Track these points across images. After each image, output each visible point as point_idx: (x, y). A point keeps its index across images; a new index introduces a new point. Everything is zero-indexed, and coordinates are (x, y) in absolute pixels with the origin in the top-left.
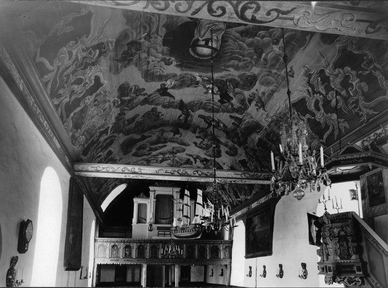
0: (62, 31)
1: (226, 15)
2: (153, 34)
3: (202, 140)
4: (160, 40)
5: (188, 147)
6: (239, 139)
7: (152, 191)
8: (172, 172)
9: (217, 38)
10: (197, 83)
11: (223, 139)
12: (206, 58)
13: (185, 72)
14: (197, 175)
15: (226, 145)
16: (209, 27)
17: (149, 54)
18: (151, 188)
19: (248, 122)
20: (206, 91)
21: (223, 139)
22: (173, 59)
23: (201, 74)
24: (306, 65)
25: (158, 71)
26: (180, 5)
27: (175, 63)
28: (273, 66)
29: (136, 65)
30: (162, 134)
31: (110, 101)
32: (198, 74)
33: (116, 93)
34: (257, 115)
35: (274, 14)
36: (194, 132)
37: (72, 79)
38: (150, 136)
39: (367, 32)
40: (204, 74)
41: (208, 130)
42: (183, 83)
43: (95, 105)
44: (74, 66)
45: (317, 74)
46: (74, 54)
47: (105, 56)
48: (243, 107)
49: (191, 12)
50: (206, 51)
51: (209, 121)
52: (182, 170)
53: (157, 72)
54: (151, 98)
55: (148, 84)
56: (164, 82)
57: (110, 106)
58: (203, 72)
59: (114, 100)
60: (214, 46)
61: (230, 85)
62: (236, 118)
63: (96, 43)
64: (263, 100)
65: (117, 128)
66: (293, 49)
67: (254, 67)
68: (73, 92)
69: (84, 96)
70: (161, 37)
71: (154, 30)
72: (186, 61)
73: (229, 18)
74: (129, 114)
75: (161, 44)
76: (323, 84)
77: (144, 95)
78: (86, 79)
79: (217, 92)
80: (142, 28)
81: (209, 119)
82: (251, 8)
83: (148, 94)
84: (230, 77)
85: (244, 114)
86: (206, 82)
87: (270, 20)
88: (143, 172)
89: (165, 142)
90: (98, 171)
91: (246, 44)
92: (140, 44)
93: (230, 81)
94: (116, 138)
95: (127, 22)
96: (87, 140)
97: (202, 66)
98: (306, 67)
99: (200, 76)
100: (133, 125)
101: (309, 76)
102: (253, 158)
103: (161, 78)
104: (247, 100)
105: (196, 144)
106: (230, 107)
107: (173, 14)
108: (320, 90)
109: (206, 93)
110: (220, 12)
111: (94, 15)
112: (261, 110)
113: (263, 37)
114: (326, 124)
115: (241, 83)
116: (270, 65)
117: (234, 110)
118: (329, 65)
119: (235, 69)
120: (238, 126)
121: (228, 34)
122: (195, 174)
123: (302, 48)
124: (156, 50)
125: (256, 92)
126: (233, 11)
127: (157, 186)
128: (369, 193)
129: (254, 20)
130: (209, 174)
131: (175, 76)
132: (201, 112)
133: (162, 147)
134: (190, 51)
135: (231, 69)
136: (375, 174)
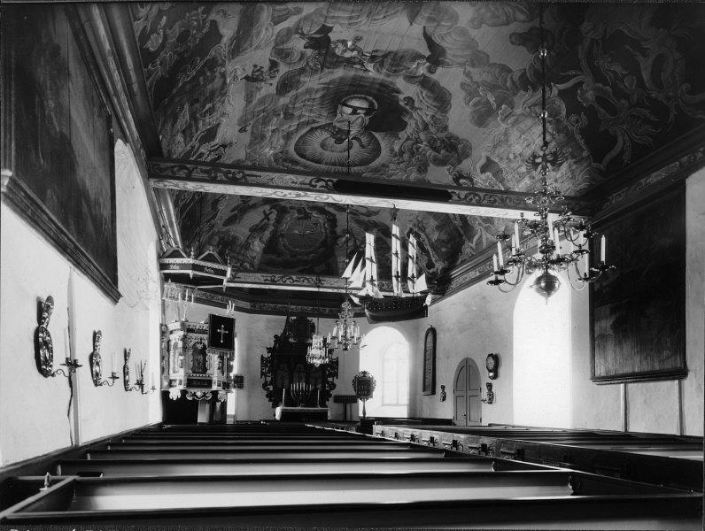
4: (409, 130)
10: (373, 58)
13: (390, 79)
17: (426, 126)
20: (359, 44)
22: (402, 103)
27: (401, 97)
40: (361, 73)
50: (356, 103)
53: (429, 97)
60: (345, 109)
85: (274, 37)
99: (366, 70)
103: (425, 83)
109: (357, 39)
124: (416, 124)
125: (271, 82)
135: (316, 87)
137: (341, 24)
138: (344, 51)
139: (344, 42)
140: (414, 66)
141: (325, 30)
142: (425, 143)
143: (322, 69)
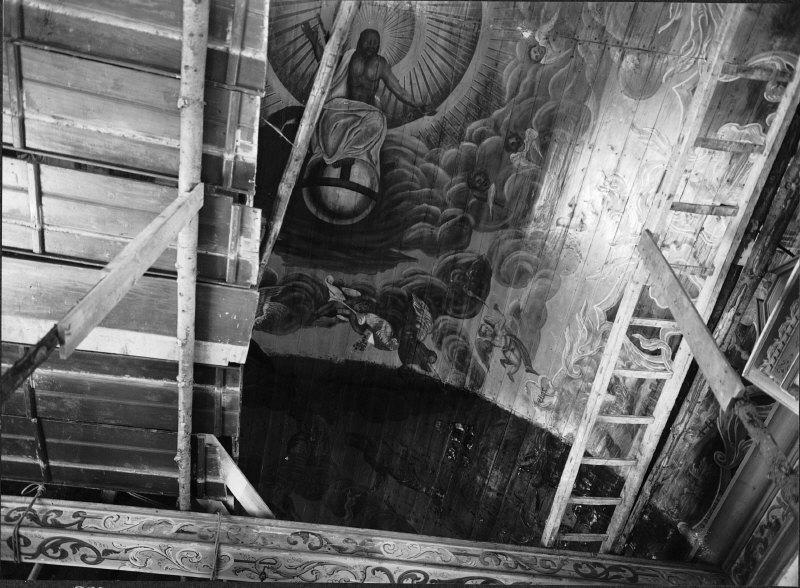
9: (370, 157)
10: (333, 310)
12: (349, 222)
13: (296, 270)
20: (359, 339)
50: (345, 198)
61: (420, 310)
67: (474, 232)
86: (357, 306)
113: (480, 137)
138: (378, 327)
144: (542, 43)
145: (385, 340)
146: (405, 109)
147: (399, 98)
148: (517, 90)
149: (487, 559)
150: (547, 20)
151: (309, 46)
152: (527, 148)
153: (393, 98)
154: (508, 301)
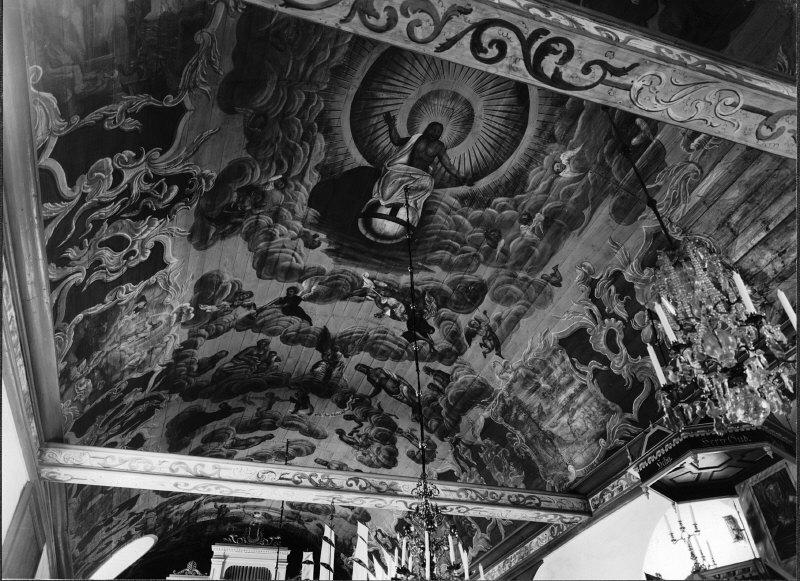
0: (115, 122)
1: (506, 62)
2: (293, 179)
3: (356, 425)
4: (303, 195)
5: (323, 442)
6: (440, 420)
7: (219, 557)
8: (296, 478)
9: (416, 204)
10: (364, 293)
11: (405, 422)
12: (389, 242)
13: (342, 267)
14: (355, 487)
15: (410, 437)
16: (402, 183)
17: (277, 217)
18: (217, 549)
19: (463, 383)
20: (379, 311)
21: (405, 422)
22: (323, 236)
23: (375, 273)
24: (585, 263)
25: (286, 259)
26: (419, 23)
27: (324, 245)
28: (519, 264)
29: (247, 239)
30: (270, 408)
31: (172, 308)
32: (367, 274)
33: (188, 293)
34: (485, 365)
35: (597, 71)
36: (341, 405)
37: (106, 233)
38: (241, 409)
39: (759, 136)
40: (379, 275)
41: (373, 400)
42: (336, 290)
43: (137, 310)
44: (118, 206)
45: (608, 278)
46: (126, 178)
47: (187, 204)
48: (454, 348)
49: (436, 43)
50: (391, 228)
51: (380, 382)
52: (320, 475)
53: (286, 259)
54: (261, 317)
55: (263, 283)
56: (295, 284)
57: (169, 319)
58: (377, 270)
59: (181, 309)
61: (430, 302)
62: (437, 374)
63: (177, 170)
64: (497, 333)
65: (170, 379)
66: (558, 232)
67: (481, 265)
68: (97, 264)
69: (120, 282)
70: (307, 187)
71: (296, 172)
72: (347, 245)
73: (510, 68)
74: (205, 349)
75: (305, 202)
76: (621, 298)
77: (249, 307)
78: (134, 242)
79: (402, 314)
80: (274, 164)
81: (377, 376)
82: (556, 52)
83: (258, 306)
84: (432, 285)
85: (455, 365)
86: (383, 293)
87: (589, 84)
88: (224, 475)
89: (273, 427)
90: (106, 469)
91: (470, 221)
92: (264, 194)
93: (432, 292)
94: (163, 405)
95: (247, 144)
96: (95, 394)
97: (376, 256)
98: (584, 266)
99: (372, 279)
100: (208, 375)
101: (592, 284)
102: (471, 465)
103: (291, 273)
104: (463, 334)
105: (341, 433)
106: (427, 347)
107: (399, 43)
108: (616, 309)
109: (380, 316)
110: (493, 52)
111: (188, 114)
112: (493, 356)
113: (503, 208)
114: (635, 379)
115: (454, 297)
116: (514, 262)
117: (435, 355)
118: (630, 262)
119: (444, 269)
120: (440, 392)
121: (436, 198)
122: (351, 485)
123: (577, 231)
124: (293, 212)
125: (482, 317)
126: (519, 53)
127: (230, 543)
128: (770, 525)
129: (556, 80)
130: (384, 488)
131: (320, 272)
132: (364, 357)
133: (263, 439)
134: (360, 225)
135: (437, 268)
136: (771, 480)
137: (394, 335)
138: (395, 306)
139: (393, 316)
140: (314, 288)
141: (410, 336)
142: (271, 187)
143: (424, 293)
144: (564, 162)
145: (399, 315)
146: (450, 178)
147: (447, 170)
148: (537, 186)
149: (461, 494)
150: (572, 149)
151: (386, 128)
152: (533, 225)
153: (443, 170)
154: (109, 343)
